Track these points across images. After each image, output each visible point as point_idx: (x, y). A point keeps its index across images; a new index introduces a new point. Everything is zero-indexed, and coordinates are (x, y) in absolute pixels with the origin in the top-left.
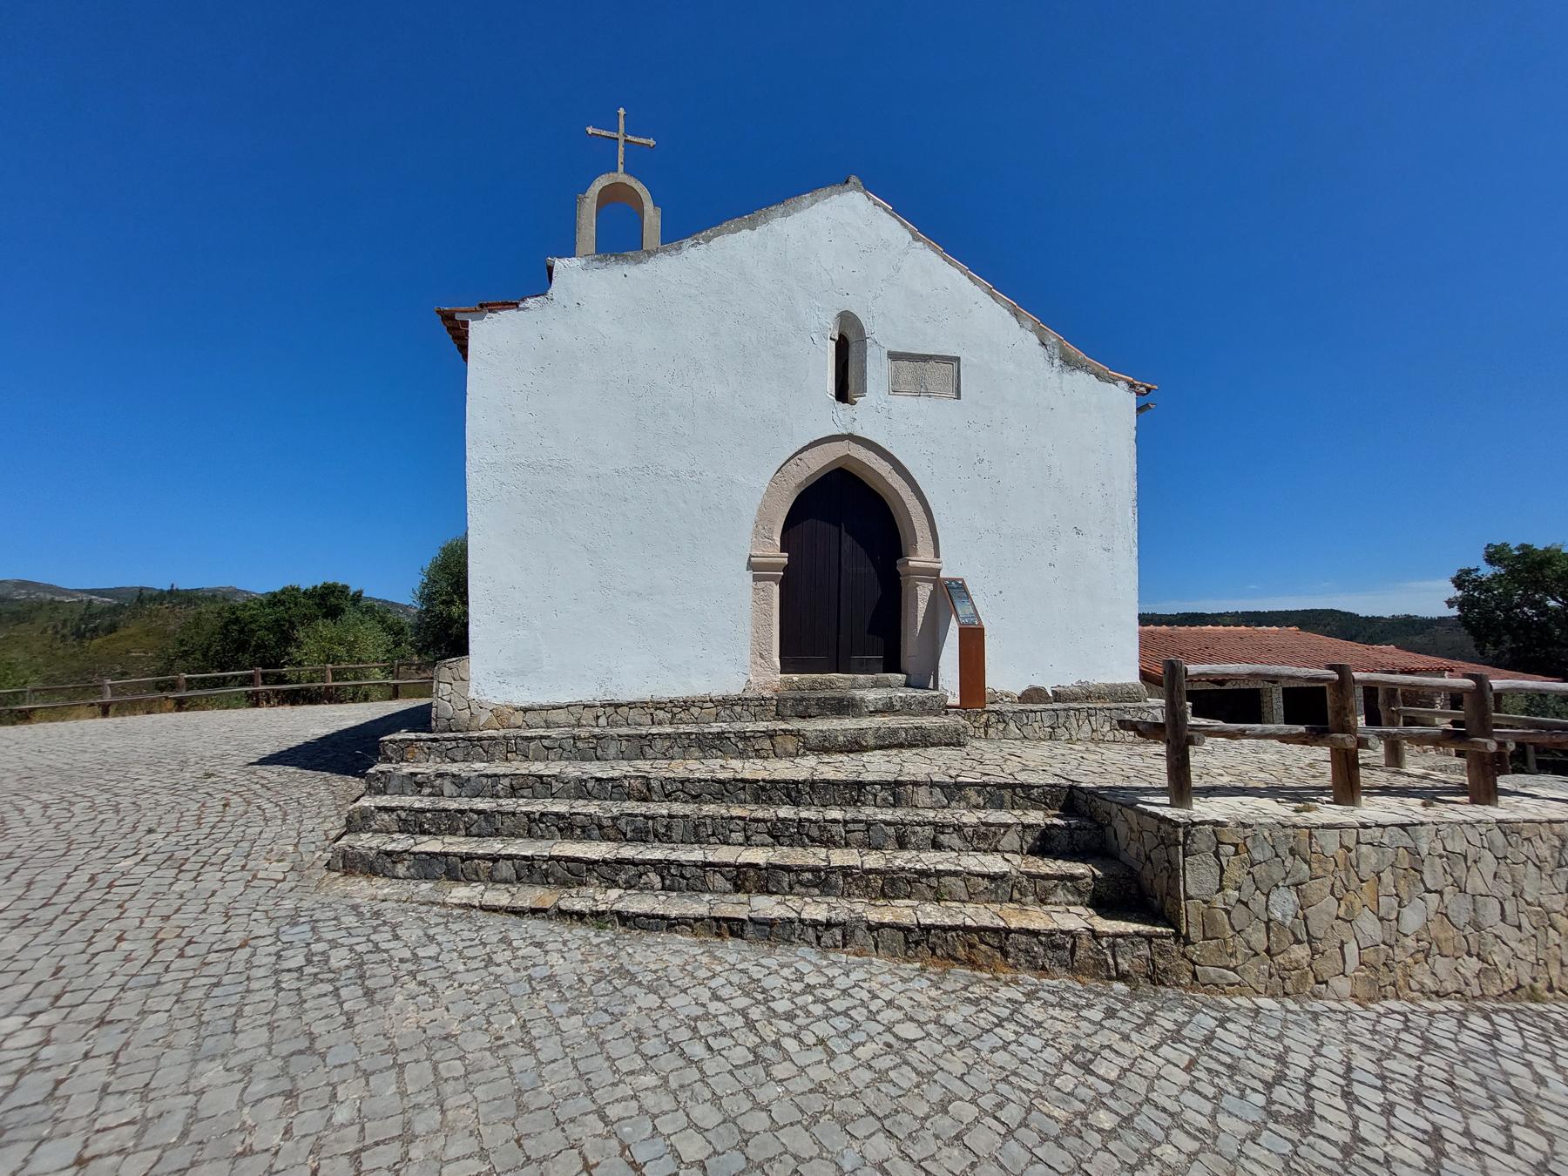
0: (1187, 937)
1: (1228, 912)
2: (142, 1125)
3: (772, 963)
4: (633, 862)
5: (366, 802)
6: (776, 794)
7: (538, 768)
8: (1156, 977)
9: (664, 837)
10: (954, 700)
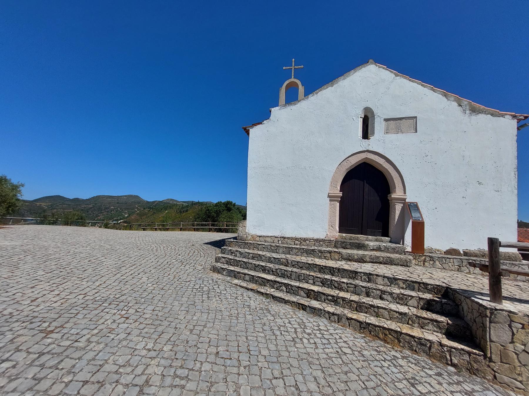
2: (163, 308)
3: (312, 320)
4: (278, 282)
5: (220, 255)
6: (326, 271)
7: (260, 253)
8: (473, 371)
9: (290, 278)
10: (409, 249)
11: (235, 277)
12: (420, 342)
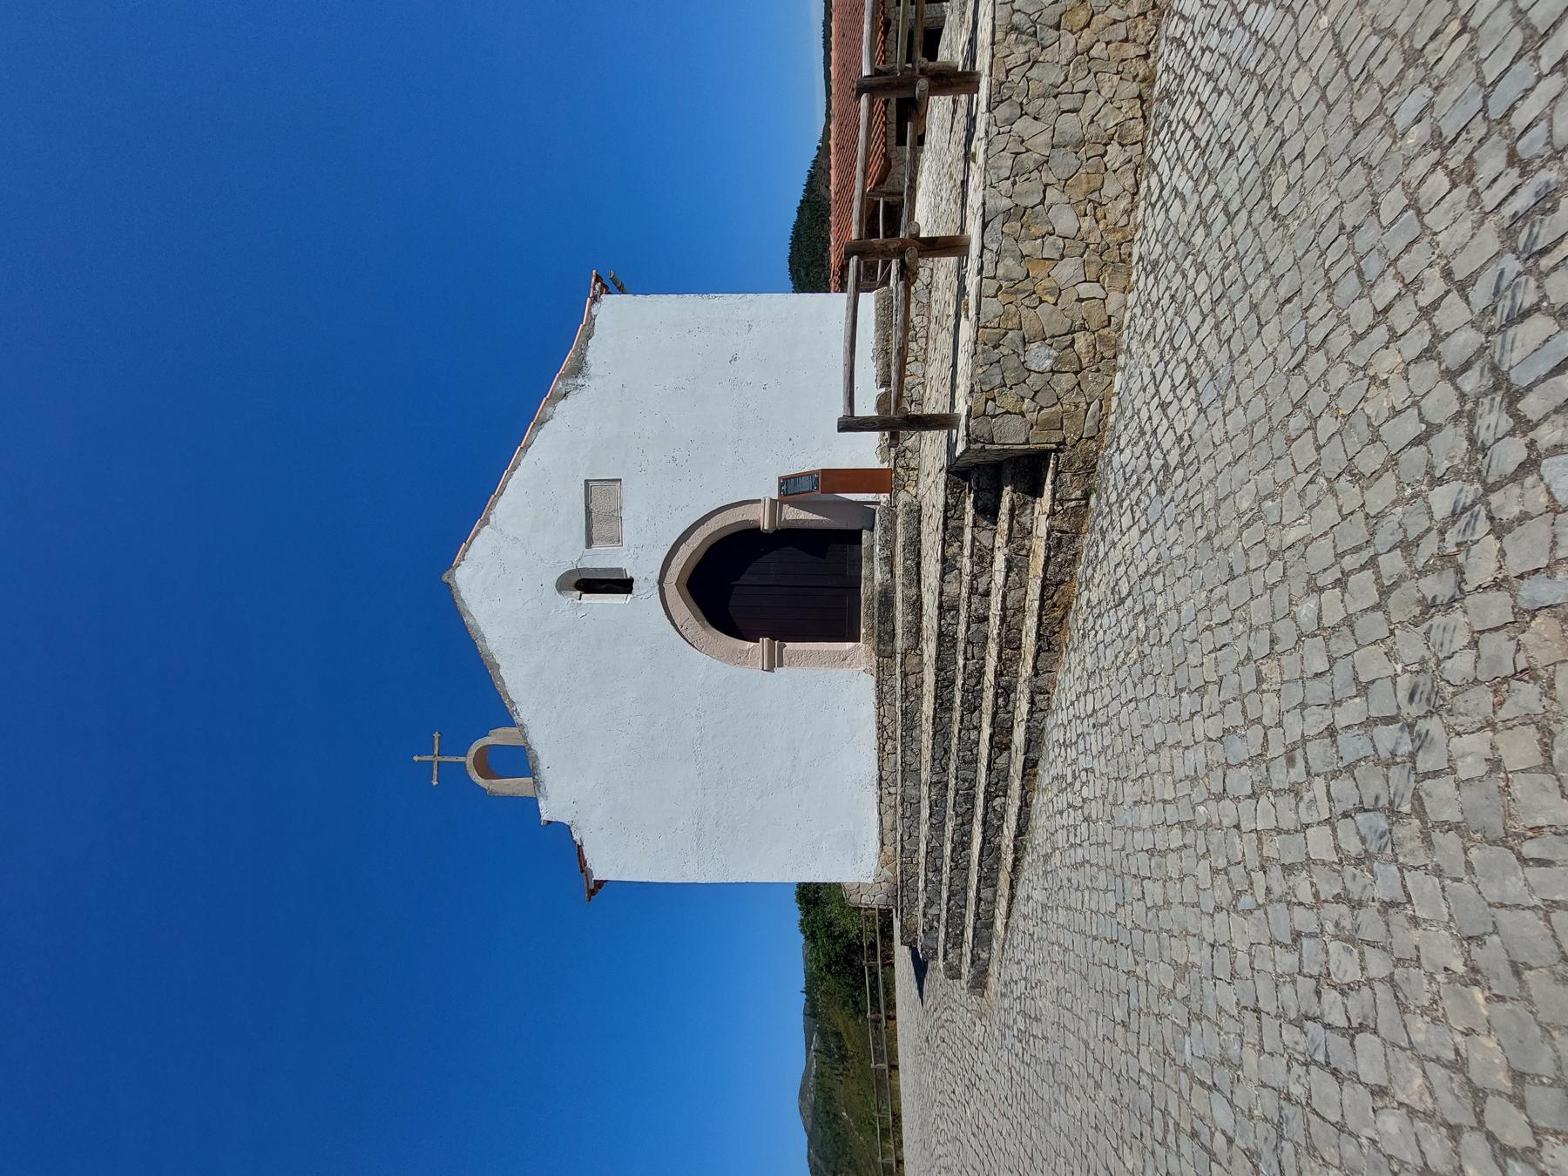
0: (1059, 444)
1: (1042, 408)
5: (941, 964)
9: (972, 783)
10: (883, 498)
11: (990, 925)
12: (1056, 544)
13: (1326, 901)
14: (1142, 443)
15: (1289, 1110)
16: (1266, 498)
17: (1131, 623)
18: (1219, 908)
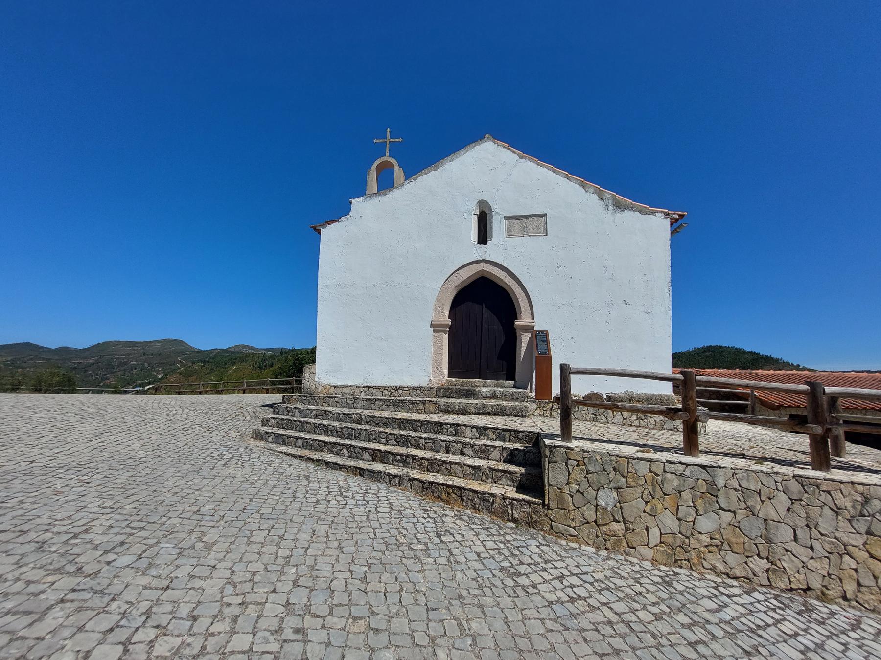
0: (548, 505)
1: (572, 496)
8: (532, 524)
9: (358, 438)
10: (534, 394)
12: (485, 497)
13: (206, 640)
14: (540, 560)
15: (107, 599)
16: (474, 640)
17: (423, 540)
18: (233, 573)
